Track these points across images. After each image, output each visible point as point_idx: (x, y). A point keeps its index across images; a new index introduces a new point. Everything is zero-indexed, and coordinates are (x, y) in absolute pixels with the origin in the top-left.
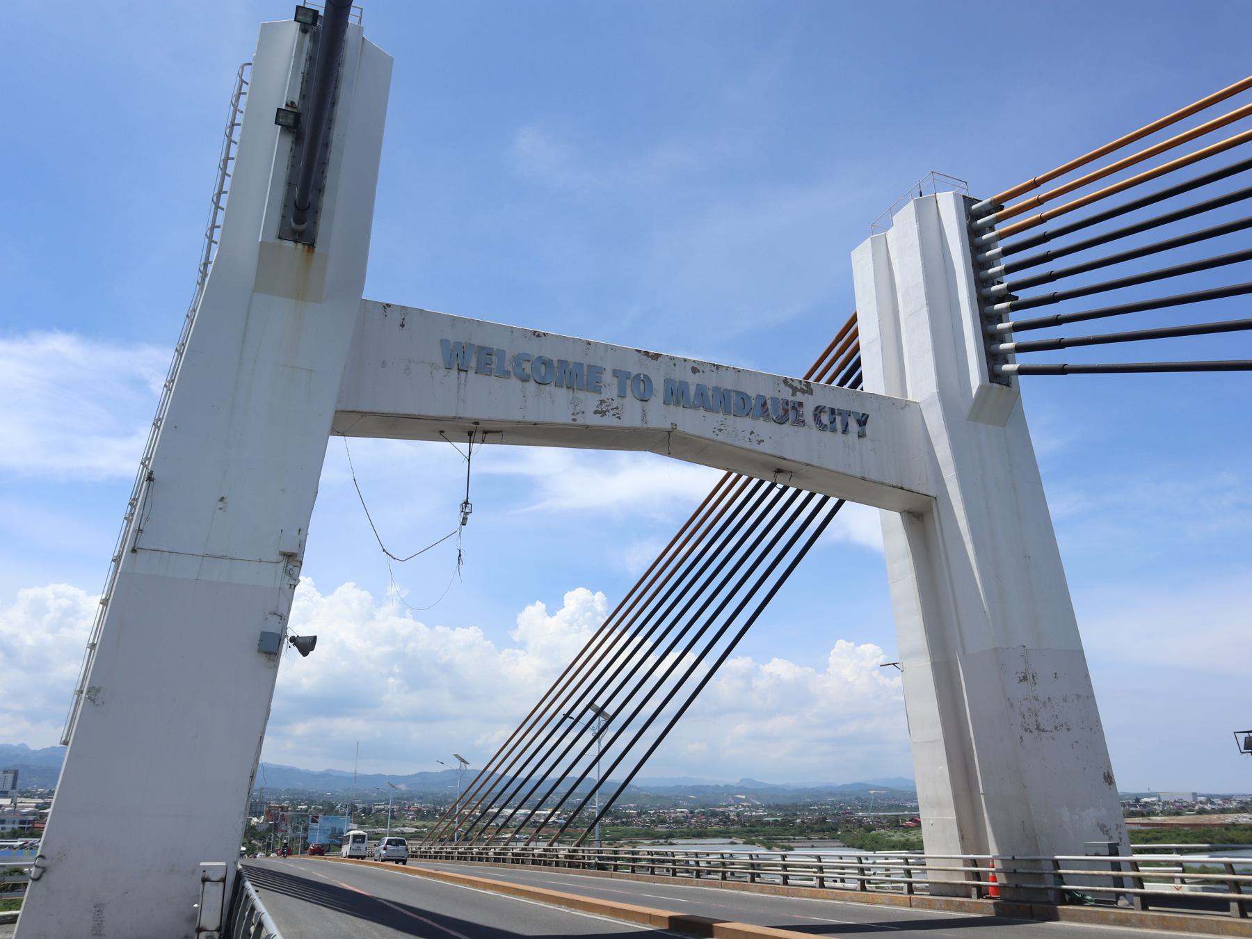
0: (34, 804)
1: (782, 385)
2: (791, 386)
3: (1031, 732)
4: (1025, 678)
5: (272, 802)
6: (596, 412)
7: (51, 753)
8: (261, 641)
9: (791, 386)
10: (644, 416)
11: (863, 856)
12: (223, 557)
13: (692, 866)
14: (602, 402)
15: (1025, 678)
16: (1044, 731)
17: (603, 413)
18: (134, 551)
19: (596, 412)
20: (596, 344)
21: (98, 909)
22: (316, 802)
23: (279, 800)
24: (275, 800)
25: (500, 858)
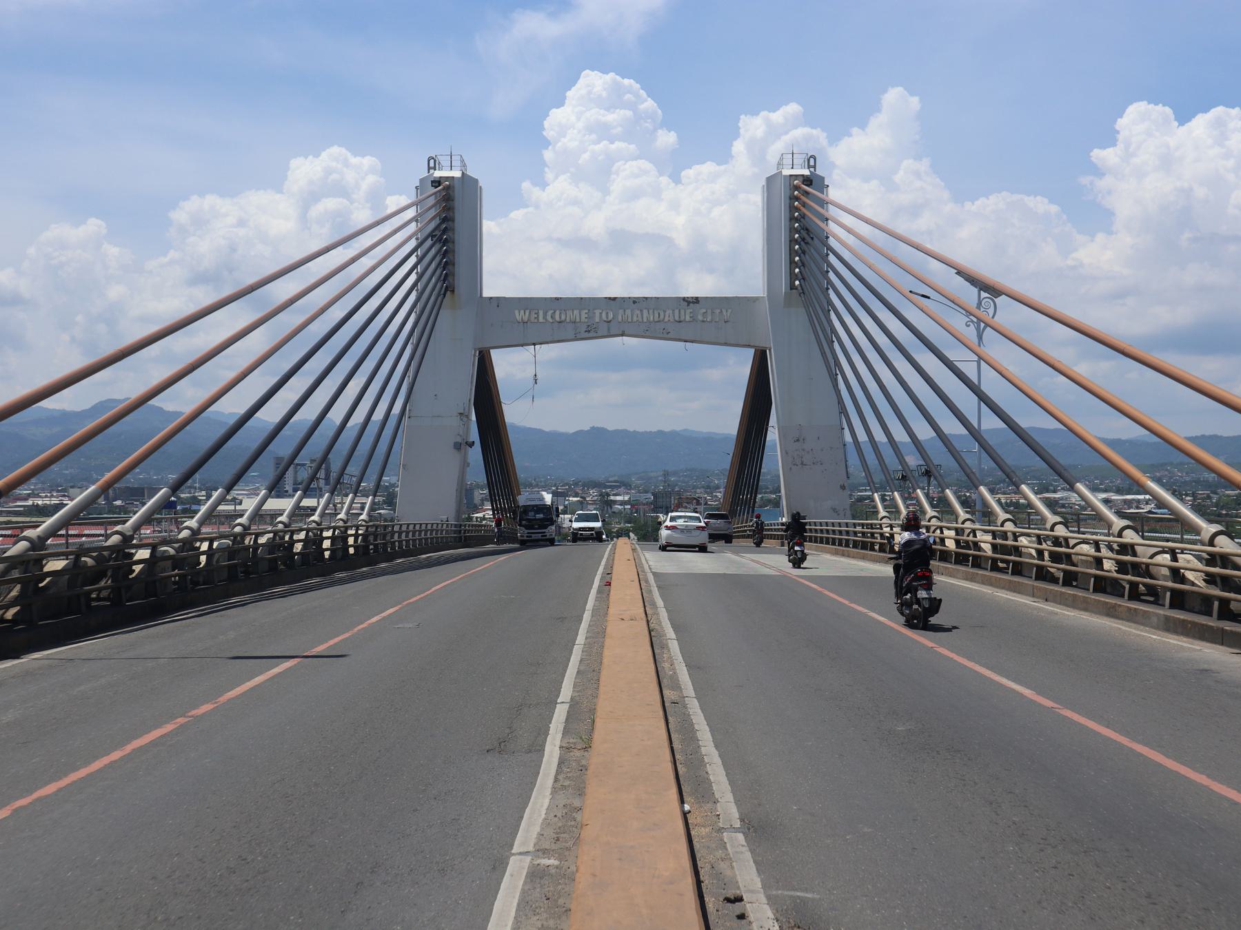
0: (359, 505)
1: (682, 301)
2: (687, 301)
3: (797, 465)
4: (798, 440)
5: (698, 491)
6: (586, 331)
7: (827, 195)
8: (454, 446)
9: (687, 301)
10: (609, 329)
11: (1009, 531)
12: (439, 416)
13: (868, 538)
14: (588, 326)
15: (798, 440)
16: (805, 465)
17: (589, 331)
18: (409, 417)
19: (586, 331)
20: (585, 298)
21: (1082, 895)
22: (768, 488)
23: (708, 487)
24: (703, 487)
25: (968, 555)
